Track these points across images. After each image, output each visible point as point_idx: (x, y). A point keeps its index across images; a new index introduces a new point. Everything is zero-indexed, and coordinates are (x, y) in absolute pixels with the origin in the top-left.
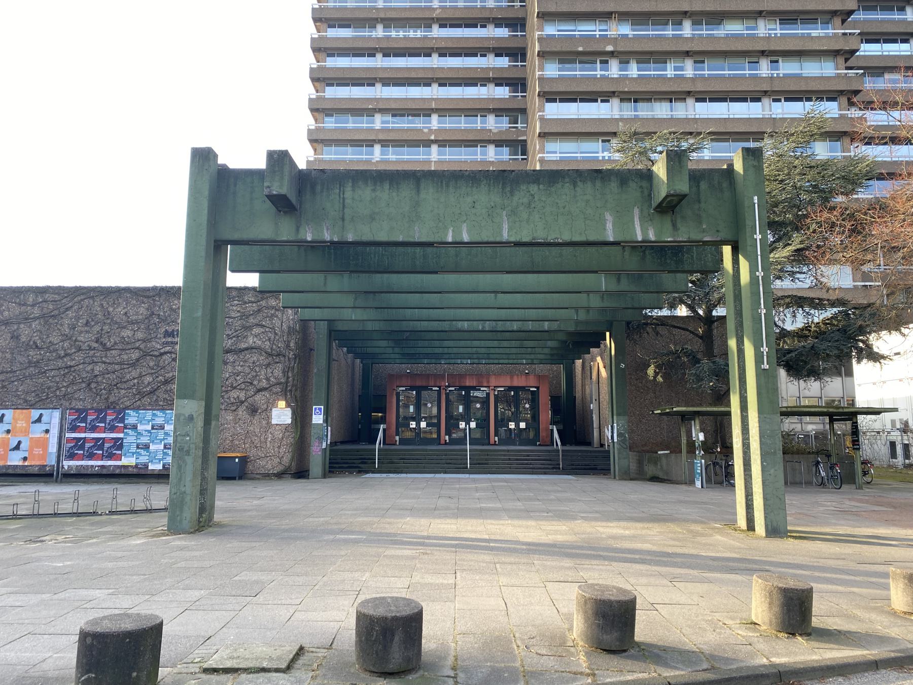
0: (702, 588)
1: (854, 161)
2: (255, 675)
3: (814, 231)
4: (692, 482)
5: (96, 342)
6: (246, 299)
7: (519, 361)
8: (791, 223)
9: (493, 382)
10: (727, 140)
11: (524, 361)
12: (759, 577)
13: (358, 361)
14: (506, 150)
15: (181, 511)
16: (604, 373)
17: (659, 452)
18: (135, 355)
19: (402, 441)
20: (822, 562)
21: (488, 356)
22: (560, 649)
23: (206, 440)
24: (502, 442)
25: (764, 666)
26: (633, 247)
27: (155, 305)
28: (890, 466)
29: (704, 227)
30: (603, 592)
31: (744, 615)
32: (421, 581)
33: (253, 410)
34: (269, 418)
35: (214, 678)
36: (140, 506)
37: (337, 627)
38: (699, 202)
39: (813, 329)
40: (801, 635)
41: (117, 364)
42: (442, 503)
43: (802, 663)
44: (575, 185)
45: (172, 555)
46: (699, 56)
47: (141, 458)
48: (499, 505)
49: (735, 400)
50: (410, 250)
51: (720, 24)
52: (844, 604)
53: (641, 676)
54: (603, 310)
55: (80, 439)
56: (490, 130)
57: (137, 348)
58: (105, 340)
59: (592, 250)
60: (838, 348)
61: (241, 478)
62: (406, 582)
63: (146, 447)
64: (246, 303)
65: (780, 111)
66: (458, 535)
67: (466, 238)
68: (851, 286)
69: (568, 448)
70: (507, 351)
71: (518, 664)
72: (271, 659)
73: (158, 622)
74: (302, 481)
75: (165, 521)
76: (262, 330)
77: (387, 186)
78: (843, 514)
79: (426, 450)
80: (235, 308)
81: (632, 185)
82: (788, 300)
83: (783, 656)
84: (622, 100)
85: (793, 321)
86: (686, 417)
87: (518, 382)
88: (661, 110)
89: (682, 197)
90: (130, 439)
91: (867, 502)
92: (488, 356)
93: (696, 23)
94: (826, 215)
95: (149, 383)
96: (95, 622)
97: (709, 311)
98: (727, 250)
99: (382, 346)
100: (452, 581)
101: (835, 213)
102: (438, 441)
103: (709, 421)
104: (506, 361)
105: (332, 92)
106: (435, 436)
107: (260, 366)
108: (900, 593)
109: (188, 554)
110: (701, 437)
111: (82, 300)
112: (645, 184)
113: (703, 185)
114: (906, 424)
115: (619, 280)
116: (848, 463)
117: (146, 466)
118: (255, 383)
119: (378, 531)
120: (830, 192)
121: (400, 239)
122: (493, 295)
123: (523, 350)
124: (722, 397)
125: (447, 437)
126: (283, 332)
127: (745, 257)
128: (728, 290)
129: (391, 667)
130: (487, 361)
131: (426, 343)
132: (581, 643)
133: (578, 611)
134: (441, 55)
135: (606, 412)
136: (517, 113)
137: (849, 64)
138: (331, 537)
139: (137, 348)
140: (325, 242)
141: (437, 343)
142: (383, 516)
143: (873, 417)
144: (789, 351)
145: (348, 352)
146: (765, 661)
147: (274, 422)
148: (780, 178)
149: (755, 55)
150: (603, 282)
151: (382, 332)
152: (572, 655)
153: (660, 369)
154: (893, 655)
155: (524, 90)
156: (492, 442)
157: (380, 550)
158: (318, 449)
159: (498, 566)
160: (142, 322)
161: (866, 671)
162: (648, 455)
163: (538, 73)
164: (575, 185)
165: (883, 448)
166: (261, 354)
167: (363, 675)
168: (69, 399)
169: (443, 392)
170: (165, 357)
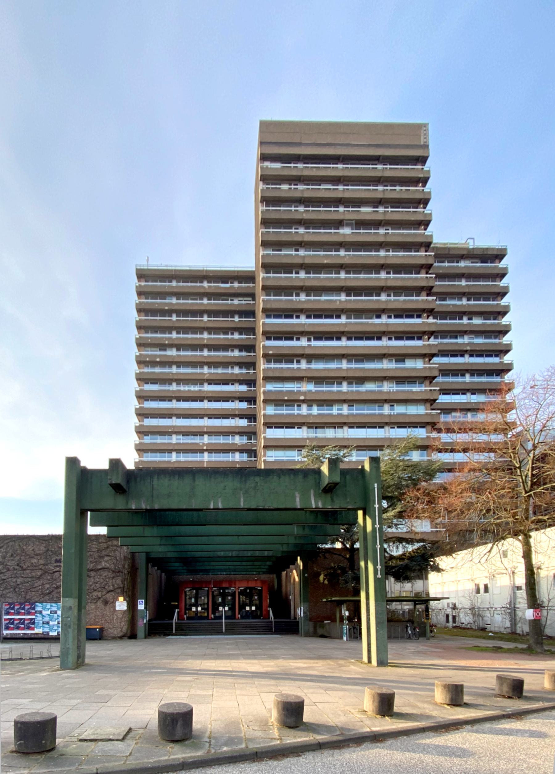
0: (341, 693)
1: (431, 462)
2: (106, 743)
3: (408, 502)
4: (342, 638)
5: (18, 566)
6: (100, 541)
7: (253, 573)
8: (397, 497)
9: (238, 585)
10: (365, 450)
11: (255, 573)
12: (369, 688)
13: (163, 574)
14: (245, 455)
15: (67, 658)
16: (297, 579)
17: (325, 622)
18: (39, 573)
19: (188, 618)
20: (404, 679)
21: (235, 570)
22: (265, 727)
23: (79, 619)
24: (242, 617)
25: (368, 732)
26: (311, 512)
27: (49, 545)
28: (446, 627)
29: (348, 500)
30: (287, 697)
31: (360, 707)
32: (195, 693)
33: (106, 603)
34: (114, 607)
35: (85, 744)
36: (45, 655)
37: (149, 718)
38: (346, 486)
39: (407, 555)
40: (388, 716)
41: (30, 578)
42: (208, 651)
43: (386, 730)
44: (280, 477)
45: (63, 681)
46: (351, 402)
47: (45, 629)
48: (239, 652)
49: (363, 594)
50: (190, 513)
51: (363, 384)
52: (412, 700)
53: (305, 739)
54: (296, 545)
55: (11, 619)
56: (237, 444)
57: (41, 569)
58: (22, 565)
59: (290, 512)
60: (419, 565)
61: (100, 639)
62: (186, 694)
63: (48, 623)
64: (100, 543)
65: (394, 434)
66: (216, 669)
67: (220, 506)
68: (429, 531)
69: (277, 620)
70: (245, 567)
71: (242, 735)
72: (114, 734)
73: (54, 716)
74: (133, 641)
75: (59, 663)
76: (110, 558)
77: (177, 477)
78: (419, 653)
79: (201, 623)
80: (94, 546)
81: (310, 478)
82: (394, 539)
83: (377, 727)
84: (309, 427)
85: (397, 551)
86: (339, 603)
87: (252, 584)
88: (330, 433)
89: (336, 484)
90: (39, 619)
91: (431, 647)
92: (235, 570)
93: (350, 383)
94: (415, 492)
95: (48, 589)
96: (21, 716)
97: (352, 545)
98: (360, 513)
99: (176, 565)
100: (211, 693)
101: (420, 492)
102: (207, 618)
103: (351, 604)
104: (245, 573)
105: (150, 422)
106: (206, 615)
107: (109, 578)
108: (439, 693)
109: (71, 681)
110: (347, 613)
111: (9, 542)
112: (317, 476)
113: (348, 477)
114: (455, 605)
115: (304, 529)
116: (423, 626)
117: (48, 633)
118: (106, 587)
119: (173, 667)
120: (418, 480)
121: (184, 507)
122: (237, 537)
123: (254, 567)
124: (358, 593)
125: (213, 616)
126: (121, 559)
127: (370, 517)
128: (361, 536)
129: (177, 738)
130: (235, 573)
131: (201, 564)
132: (276, 724)
133: (274, 708)
134: (209, 401)
135: (298, 600)
136: (251, 434)
137: (433, 407)
138: (148, 671)
139: (41, 569)
140: (142, 509)
141: (206, 564)
142: (176, 659)
143: (438, 602)
144: (394, 567)
145: (158, 569)
146: (368, 730)
147: (117, 608)
148: (391, 472)
149: (381, 402)
150: (295, 530)
151: (176, 558)
152: (271, 729)
153: (327, 577)
154: (432, 725)
155: (255, 422)
156: (237, 617)
157: (174, 677)
158: (142, 623)
159: (236, 685)
160: (43, 554)
161: (419, 732)
162: (319, 623)
163: (262, 412)
164: (280, 477)
165: (442, 618)
166: (109, 572)
167: (162, 742)
168: (5, 597)
169: (210, 590)
170: (56, 574)
